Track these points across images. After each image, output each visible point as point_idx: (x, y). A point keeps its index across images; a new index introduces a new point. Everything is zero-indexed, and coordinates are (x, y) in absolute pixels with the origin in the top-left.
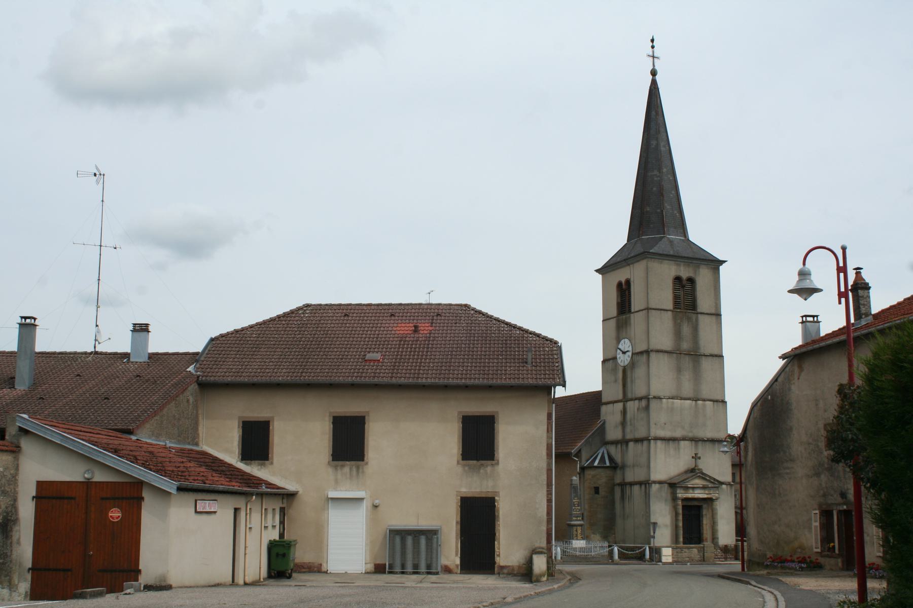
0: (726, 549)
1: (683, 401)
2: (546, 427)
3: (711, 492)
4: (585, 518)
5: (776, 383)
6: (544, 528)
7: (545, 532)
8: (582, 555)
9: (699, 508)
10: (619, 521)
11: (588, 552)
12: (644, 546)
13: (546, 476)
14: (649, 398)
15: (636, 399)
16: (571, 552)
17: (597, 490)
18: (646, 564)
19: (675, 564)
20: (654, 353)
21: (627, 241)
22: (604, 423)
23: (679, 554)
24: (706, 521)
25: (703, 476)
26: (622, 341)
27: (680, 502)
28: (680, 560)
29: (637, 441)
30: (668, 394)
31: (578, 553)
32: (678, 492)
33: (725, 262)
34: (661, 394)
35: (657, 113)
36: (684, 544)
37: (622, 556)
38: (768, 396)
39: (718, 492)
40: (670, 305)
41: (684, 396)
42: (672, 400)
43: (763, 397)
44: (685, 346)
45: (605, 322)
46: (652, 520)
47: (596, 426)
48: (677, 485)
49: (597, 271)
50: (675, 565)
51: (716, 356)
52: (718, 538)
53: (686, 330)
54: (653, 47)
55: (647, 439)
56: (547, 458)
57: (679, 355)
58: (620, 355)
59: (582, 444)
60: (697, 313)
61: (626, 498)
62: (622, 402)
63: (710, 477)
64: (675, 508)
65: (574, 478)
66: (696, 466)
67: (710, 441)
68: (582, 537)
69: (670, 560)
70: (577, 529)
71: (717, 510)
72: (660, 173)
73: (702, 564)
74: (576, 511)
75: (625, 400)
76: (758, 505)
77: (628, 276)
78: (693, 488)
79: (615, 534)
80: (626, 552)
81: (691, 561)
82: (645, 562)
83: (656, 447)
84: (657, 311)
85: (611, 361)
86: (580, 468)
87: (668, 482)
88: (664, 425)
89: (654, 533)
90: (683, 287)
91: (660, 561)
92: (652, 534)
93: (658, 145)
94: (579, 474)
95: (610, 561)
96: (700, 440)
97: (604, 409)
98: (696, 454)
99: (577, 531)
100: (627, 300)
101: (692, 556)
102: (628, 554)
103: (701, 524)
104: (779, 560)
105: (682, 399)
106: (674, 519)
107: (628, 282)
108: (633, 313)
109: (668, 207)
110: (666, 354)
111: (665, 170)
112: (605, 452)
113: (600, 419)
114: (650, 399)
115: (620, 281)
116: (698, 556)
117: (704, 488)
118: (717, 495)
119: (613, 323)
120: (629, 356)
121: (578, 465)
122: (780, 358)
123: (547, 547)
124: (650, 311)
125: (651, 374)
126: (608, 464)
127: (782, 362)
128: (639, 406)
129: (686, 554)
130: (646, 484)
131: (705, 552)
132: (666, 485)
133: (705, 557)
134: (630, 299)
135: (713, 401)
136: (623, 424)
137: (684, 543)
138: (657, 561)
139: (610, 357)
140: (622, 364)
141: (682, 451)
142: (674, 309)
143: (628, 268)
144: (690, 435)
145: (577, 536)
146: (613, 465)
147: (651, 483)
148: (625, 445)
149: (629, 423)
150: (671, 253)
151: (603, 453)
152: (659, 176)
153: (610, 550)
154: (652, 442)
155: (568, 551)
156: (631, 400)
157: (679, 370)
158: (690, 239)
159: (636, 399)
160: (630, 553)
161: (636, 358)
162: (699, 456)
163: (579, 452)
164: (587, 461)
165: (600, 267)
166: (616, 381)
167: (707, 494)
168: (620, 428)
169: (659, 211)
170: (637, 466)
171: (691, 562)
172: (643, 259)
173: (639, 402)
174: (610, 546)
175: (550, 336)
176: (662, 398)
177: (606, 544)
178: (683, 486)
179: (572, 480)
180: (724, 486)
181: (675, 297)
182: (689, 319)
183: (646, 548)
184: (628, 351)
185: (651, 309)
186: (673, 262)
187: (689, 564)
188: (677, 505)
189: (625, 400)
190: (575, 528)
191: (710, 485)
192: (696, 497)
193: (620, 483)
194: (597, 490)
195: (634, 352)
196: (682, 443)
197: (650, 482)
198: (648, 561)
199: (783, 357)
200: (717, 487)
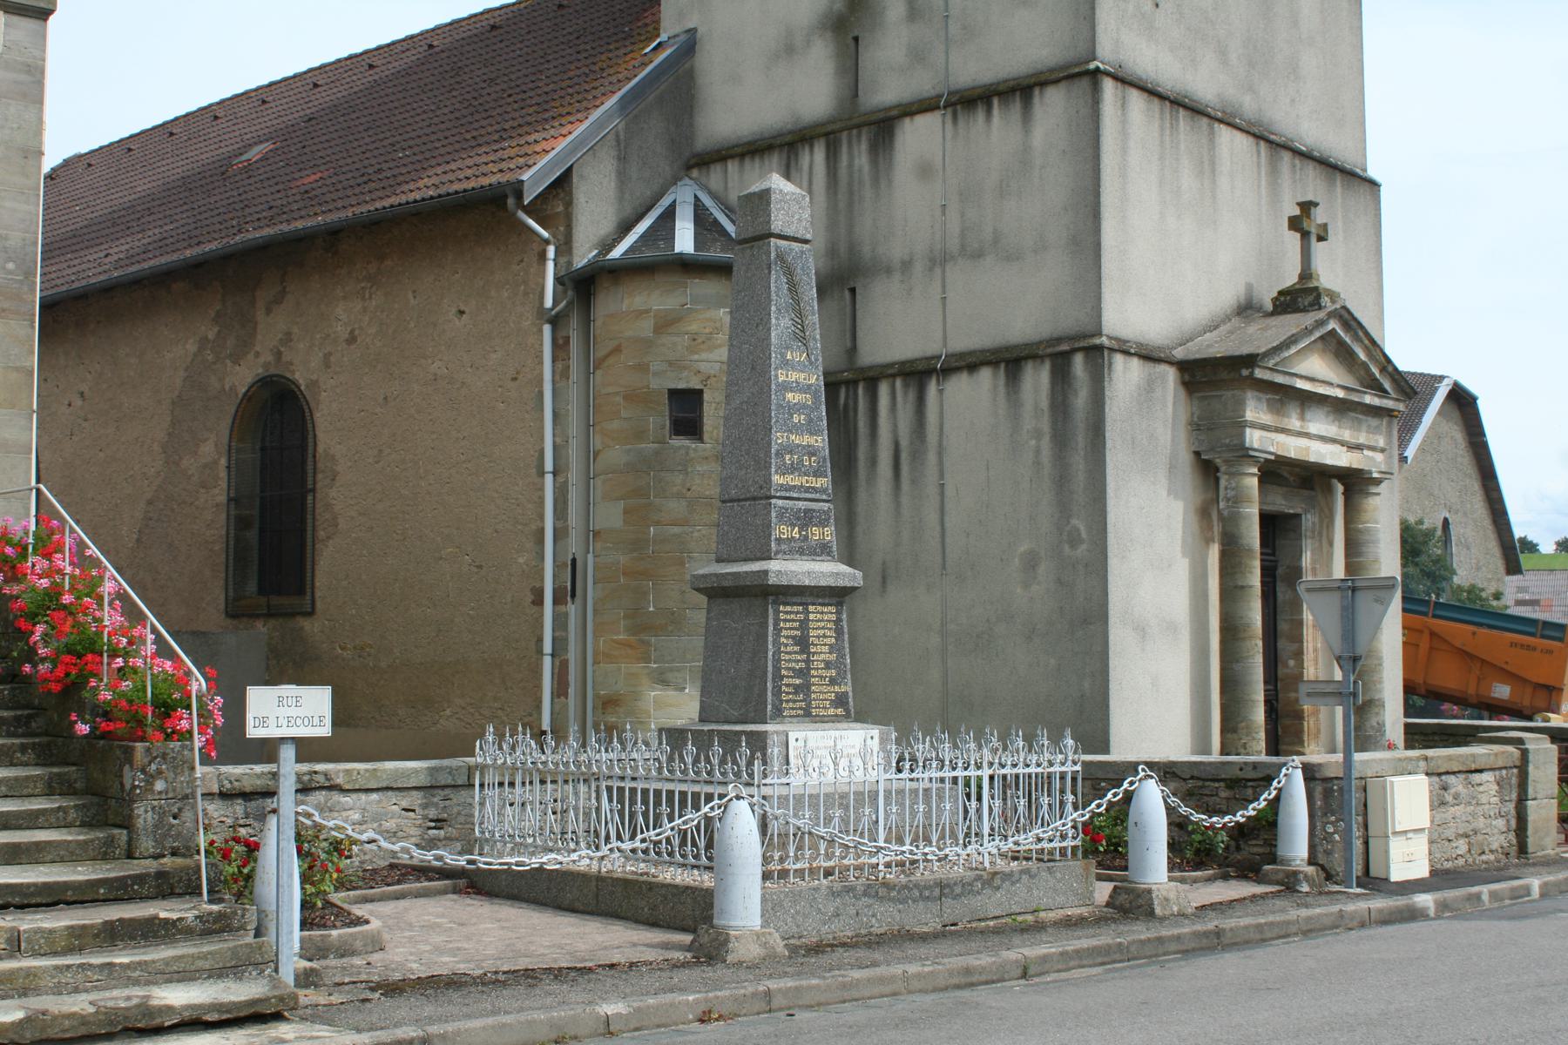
22: (689, 45)
27: (1255, 481)
32: (1250, 415)
61: (873, 461)
68: (840, 701)
70: (804, 625)
74: (793, 469)
86: (558, 280)
87: (1179, 353)
94: (556, 321)
99: (803, 643)
121: (550, 266)
132: (1171, 374)
141: (1223, 182)
145: (805, 689)
170: (978, 255)
190: (789, 615)
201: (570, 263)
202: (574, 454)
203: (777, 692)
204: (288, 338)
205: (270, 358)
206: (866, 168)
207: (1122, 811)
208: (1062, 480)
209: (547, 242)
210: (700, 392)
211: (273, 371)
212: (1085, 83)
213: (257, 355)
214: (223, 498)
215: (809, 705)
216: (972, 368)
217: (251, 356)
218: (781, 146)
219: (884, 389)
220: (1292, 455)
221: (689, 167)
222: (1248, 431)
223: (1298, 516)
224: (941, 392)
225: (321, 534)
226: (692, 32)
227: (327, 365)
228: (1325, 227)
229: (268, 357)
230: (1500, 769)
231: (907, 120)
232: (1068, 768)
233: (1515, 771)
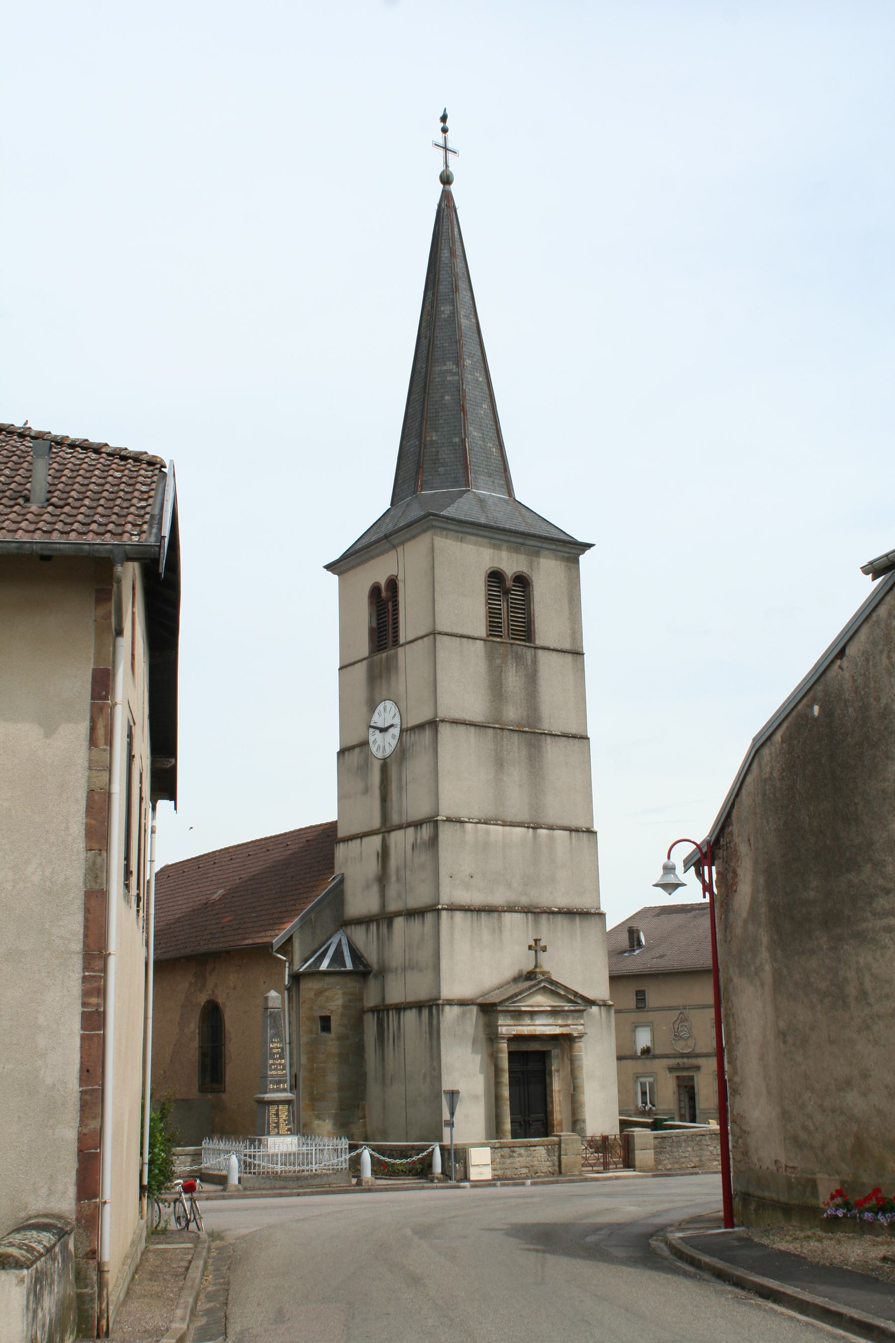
0: (602, 1145)
1: (507, 828)
2: (84, 727)
3: (569, 1022)
4: (301, 1085)
5: (838, 662)
6: (69, 1134)
7: (74, 1147)
8: (290, 1171)
9: (543, 1057)
10: (373, 1089)
11: (303, 1164)
12: (432, 1145)
13: (80, 917)
14: (437, 821)
15: (409, 825)
16: (263, 1164)
17: (325, 1023)
18: (437, 1188)
19: (499, 1183)
20: (448, 725)
21: (392, 505)
22: (342, 881)
23: (508, 1161)
24: (557, 1085)
25: (553, 988)
26: (381, 707)
27: (505, 1045)
28: (509, 1173)
29: (411, 914)
30: (476, 812)
31: (279, 1168)
32: (500, 1022)
33: (589, 546)
34: (463, 814)
35: (452, 253)
36: (513, 1138)
37: (379, 1169)
38: (811, 707)
39: (582, 1022)
40: (481, 630)
41: (510, 818)
42: (484, 826)
43: (794, 714)
44: (512, 713)
45: (344, 670)
46: (446, 1085)
47: (325, 888)
48: (499, 1008)
49: (329, 567)
50: (499, 1190)
51: (574, 737)
52: (584, 1121)
53: (513, 680)
54: (445, 130)
55: (434, 909)
56: (89, 849)
57: (499, 731)
58: (375, 737)
59: (293, 927)
60: (536, 648)
62: (377, 834)
63: (566, 988)
64: (493, 1057)
65: (273, 994)
66: (536, 966)
67: (565, 913)
68: (289, 1130)
69: (487, 1174)
70: (277, 1111)
71: (582, 1059)
72: (458, 366)
73: (557, 1182)
74: (276, 1069)
75: (386, 828)
76: (782, 1035)
77: (391, 571)
78: (532, 1014)
79: (364, 1117)
80: (388, 1160)
81: (534, 1174)
82: (432, 1181)
83: (452, 928)
84: (454, 638)
85: (357, 750)
86: (288, 975)
87: (478, 1001)
88: (468, 878)
89: (452, 1114)
90: (507, 592)
91: (466, 1178)
92: (446, 1116)
93: (454, 314)
94: (289, 989)
95: (354, 1181)
96: (544, 912)
97: (341, 851)
98: (536, 941)
99: (277, 1115)
100: (391, 622)
101: (536, 1163)
102: (394, 1164)
103: (548, 1092)
104: (874, 1202)
105: (505, 824)
106: (493, 1081)
107: (393, 584)
108: (402, 645)
109: (476, 434)
110: (473, 729)
111: (468, 362)
112: (344, 942)
113: (333, 873)
114: (440, 825)
115: (378, 583)
116: (548, 1163)
117: (554, 1013)
118: (581, 1027)
119: (360, 672)
120: (394, 736)
121: (287, 970)
122: (866, 570)
123: (79, 1211)
124: (438, 637)
125: (440, 769)
126: (349, 966)
127: (869, 586)
128: (416, 839)
129: (521, 1159)
130: (430, 1007)
131: (563, 1152)
132: (475, 1009)
133: (563, 1166)
134: (397, 618)
135: (571, 830)
136: (382, 879)
137: (515, 1135)
138: (458, 1177)
139: (355, 742)
140: (380, 755)
142: (488, 636)
143: (393, 553)
144: (524, 901)
145: (277, 1127)
146: (361, 968)
147: (443, 1005)
148: (385, 926)
149: (393, 878)
150: (483, 520)
151: (339, 945)
152: (456, 374)
153: (351, 1156)
154: (444, 914)
155: (257, 1162)
156: (400, 827)
157: (499, 763)
158: (517, 499)
159: (409, 825)
160: (398, 1161)
161: (409, 738)
162: (542, 943)
163: (286, 947)
164: (306, 961)
165: (336, 556)
166: (366, 790)
167: (561, 1026)
168: (375, 889)
169: (456, 440)
170: (413, 969)
171: (532, 1178)
172: (424, 531)
173: (416, 832)
174: (353, 1148)
175: (134, 446)
176: (466, 822)
177: (344, 1143)
178: (512, 1009)
179: (266, 998)
180: (595, 1009)
181: (490, 612)
182: (519, 659)
183: (433, 1149)
184: (392, 726)
185: (440, 633)
186: (487, 540)
187: (529, 1182)
188: (498, 1051)
189: (386, 828)
190: (273, 1109)
191: (567, 1007)
192: (538, 1033)
193: (376, 1006)
194: (325, 1023)
195: (404, 726)
196: (507, 917)
197: (440, 1002)
198: (440, 1180)
199: (875, 569)
200: (582, 1011)
201: (293, 969)
202: (294, 1037)
203: (269, 1128)
204: (216, 986)
205: (211, 992)
206: (386, 933)
207: (359, 1156)
208: (431, 1048)
209: (286, 961)
210: (330, 1017)
211: (212, 998)
212: (436, 913)
213: (207, 991)
214: (197, 1046)
215: (279, 1131)
216: (411, 1008)
217: (205, 991)
218: (365, 922)
219: (391, 1013)
220: (526, 1033)
221: (342, 926)
222: (500, 1028)
223: (550, 1051)
224: (404, 1015)
225: (227, 1061)
226: (343, 874)
227: (228, 997)
228: (545, 947)
229: (210, 992)
230: (547, 1145)
231: (396, 918)
232: (343, 1147)
233: (557, 1146)
